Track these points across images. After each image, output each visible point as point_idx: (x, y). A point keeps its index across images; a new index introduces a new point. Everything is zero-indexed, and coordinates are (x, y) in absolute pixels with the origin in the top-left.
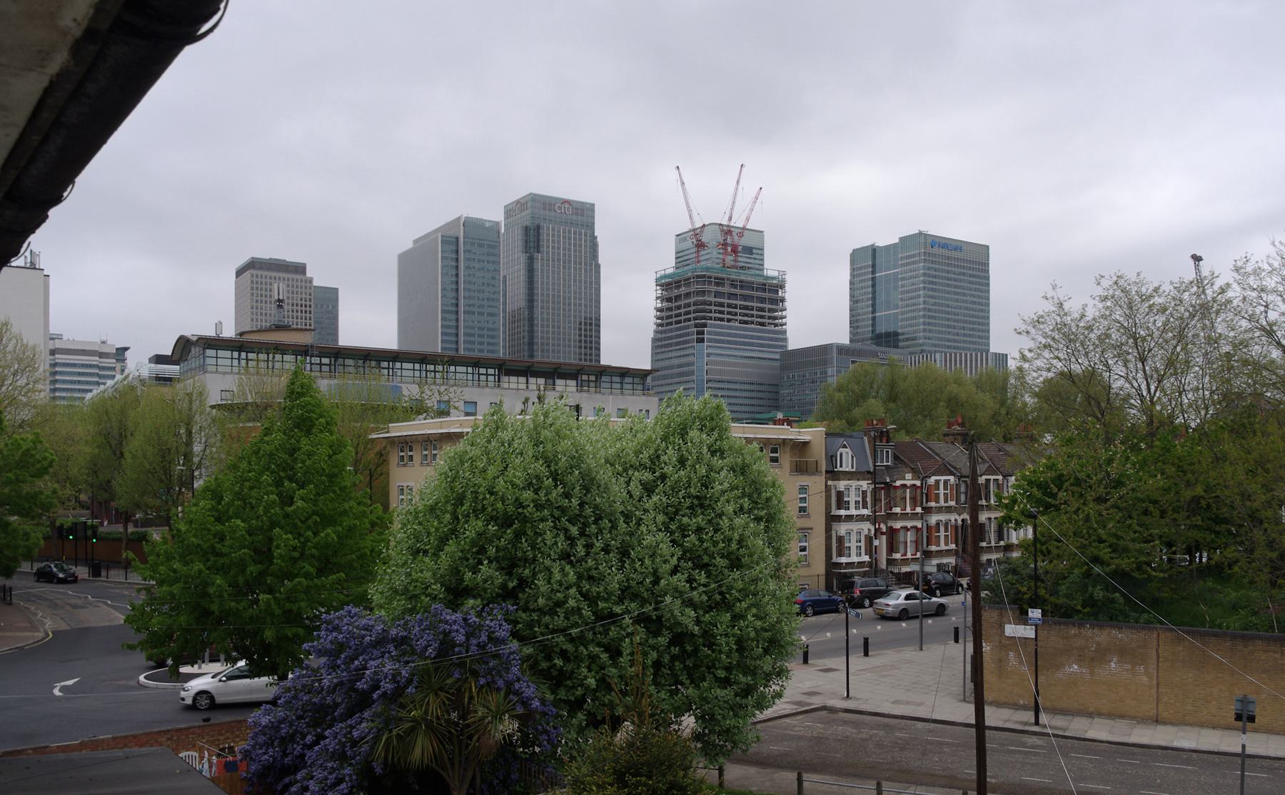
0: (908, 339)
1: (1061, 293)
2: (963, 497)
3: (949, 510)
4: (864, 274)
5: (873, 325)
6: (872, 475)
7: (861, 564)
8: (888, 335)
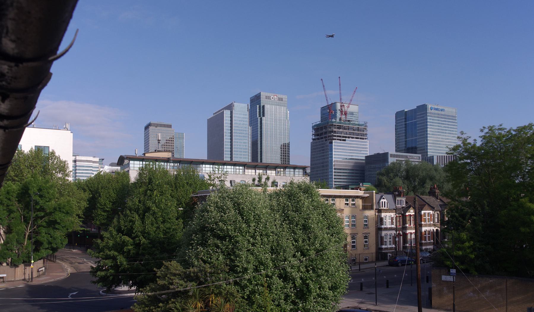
0: (421, 150)
1: (464, 136)
2: (436, 220)
3: (430, 225)
4: (402, 122)
5: (406, 144)
6: (396, 210)
7: (391, 248)
8: (412, 148)
